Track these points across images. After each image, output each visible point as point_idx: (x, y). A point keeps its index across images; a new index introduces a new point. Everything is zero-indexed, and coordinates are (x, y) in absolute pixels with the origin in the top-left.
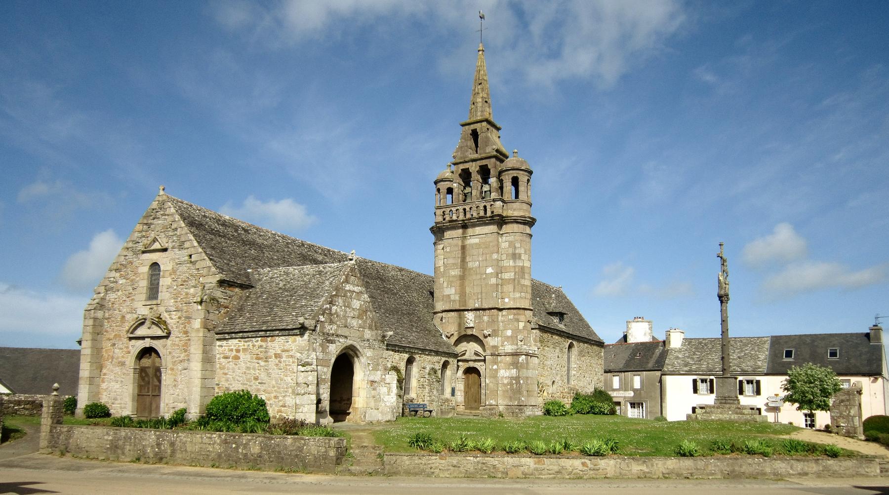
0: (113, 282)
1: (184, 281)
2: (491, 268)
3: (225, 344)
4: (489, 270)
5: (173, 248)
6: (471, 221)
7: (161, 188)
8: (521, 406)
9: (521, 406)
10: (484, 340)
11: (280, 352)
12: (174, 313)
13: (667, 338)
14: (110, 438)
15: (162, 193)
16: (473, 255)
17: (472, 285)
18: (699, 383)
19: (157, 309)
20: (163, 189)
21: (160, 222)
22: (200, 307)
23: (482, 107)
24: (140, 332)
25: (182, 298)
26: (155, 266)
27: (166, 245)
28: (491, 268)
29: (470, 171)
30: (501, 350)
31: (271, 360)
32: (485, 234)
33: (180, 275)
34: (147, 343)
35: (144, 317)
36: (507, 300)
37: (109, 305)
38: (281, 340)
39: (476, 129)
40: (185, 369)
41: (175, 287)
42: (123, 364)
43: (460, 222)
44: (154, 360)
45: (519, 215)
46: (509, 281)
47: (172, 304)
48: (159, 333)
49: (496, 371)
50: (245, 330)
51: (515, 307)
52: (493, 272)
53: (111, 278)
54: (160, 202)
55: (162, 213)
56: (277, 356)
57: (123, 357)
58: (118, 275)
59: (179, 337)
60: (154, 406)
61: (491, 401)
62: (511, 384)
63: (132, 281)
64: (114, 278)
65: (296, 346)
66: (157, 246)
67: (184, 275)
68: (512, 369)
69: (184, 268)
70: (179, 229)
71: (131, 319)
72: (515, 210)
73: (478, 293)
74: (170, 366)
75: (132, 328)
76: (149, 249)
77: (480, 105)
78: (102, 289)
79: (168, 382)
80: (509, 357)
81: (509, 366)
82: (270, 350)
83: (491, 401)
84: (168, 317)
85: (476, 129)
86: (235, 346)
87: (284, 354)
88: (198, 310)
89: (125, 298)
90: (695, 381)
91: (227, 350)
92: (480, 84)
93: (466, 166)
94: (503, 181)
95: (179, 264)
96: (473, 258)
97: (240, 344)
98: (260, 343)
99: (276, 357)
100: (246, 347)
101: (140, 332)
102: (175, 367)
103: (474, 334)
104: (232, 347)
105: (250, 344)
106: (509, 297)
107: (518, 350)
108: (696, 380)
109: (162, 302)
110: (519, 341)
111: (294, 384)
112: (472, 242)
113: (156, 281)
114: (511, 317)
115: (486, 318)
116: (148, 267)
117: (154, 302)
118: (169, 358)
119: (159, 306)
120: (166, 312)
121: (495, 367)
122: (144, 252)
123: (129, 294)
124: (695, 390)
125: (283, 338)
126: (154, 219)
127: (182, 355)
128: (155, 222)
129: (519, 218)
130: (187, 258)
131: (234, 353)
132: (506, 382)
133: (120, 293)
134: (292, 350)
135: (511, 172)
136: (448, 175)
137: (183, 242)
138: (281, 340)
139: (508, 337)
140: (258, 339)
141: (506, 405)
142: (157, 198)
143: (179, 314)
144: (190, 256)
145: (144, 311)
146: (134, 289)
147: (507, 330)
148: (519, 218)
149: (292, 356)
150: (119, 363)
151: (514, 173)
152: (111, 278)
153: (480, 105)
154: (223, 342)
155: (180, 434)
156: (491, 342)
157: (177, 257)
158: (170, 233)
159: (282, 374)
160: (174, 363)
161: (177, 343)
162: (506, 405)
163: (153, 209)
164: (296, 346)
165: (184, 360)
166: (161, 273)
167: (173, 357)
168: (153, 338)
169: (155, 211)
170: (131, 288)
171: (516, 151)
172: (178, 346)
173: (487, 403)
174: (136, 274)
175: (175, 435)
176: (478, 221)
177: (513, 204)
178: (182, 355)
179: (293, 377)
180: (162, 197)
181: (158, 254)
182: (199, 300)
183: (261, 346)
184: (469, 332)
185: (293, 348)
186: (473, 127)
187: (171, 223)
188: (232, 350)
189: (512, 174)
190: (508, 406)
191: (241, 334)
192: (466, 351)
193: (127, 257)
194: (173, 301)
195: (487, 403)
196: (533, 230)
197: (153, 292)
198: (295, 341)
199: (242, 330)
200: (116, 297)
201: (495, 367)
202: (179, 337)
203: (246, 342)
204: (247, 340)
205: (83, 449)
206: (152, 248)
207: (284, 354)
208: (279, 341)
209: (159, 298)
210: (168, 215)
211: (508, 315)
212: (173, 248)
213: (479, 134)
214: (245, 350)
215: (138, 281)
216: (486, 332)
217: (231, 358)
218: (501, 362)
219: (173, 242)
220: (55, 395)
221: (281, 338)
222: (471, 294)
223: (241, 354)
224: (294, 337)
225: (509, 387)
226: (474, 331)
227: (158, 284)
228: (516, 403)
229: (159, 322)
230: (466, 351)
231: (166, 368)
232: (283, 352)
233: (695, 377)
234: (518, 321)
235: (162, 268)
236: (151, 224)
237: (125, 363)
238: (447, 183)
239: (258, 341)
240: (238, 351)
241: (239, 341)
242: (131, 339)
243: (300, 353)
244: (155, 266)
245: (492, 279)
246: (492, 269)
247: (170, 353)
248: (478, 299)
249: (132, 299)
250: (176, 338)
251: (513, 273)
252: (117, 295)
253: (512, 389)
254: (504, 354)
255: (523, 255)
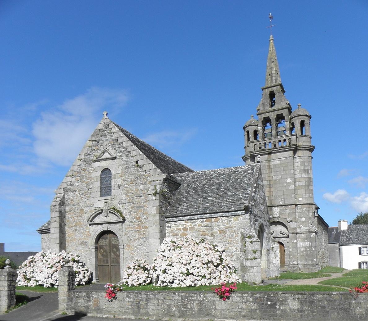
0: (71, 185)
1: (134, 180)
2: (290, 179)
3: (173, 225)
4: (289, 181)
5: (121, 156)
6: (275, 149)
7: (105, 113)
8: (313, 264)
9: (313, 264)
10: (288, 225)
11: (224, 229)
12: (127, 204)
13: (339, 225)
14: (131, 300)
15: (105, 117)
16: (276, 172)
17: (277, 190)
18: (362, 249)
19: (111, 203)
20: (107, 114)
21: (107, 138)
22: (154, 198)
23: (276, 76)
24: (96, 220)
25: (132, 193)
26: (106, 171)
27: (114, 155)
28: (290, 179)
29: (270, 118)
30: (298, 230)
31: (217, 235)
32: (285, 158)
33: (129, 176)
34: (105, 228)
35: (100, 209)
36: (300, 199)
37: (69, 202)
38: (224, 220)
39: (273, 91)
40: (140, 245)
41: (126, 186)
42: (85, 244)
43: (267, 151)
44: (110, 240)
45: (306, 145)
46: (301, 187)
47: (124, 198)
48: (115, 219)
49: (296, 243)
50: (191, 214)
51: (307, 203)
52: (291, 181)
53: (68, 182)
54: (105, 124)
55: (108, 131)
56: (221, 232)
57: (84, 239)
58: (74, 180)
59: (132, 222)
60: (113, 273)
61: (294, 262)
62: (306, 251)
63: (87, 183)
64: (71, 182)
65: (238, 223)
66: (106, 155)
67: (134, 176)
68: (306, 242)
69: (133, 170)
70: (124, 143)
71: (88, 213)
72: (303, 142)
73: (281, 195)
74: (126, 243)
75: (92, 217)
76: (99, 159)
77: (274, 75)
78: (62, 191)
79: (125, 255)
80: (304, 234)
81: (304, 240)
82: (215, 228)
83: (294, 262)
84: (121, 207)
85: (273, 91)
86: (182, 226)
87: (228, 231)
88: (153, 200)
89: (82, 196)
90: (360, 249)
91: (175, 229)
92: (273, 62)
93: (267, 115)
94: (294, 123)
95: (128, 168)
96: (276, 173)
97: (187, 225)
98: (205, 223)
99: (220, 233)
100: (193, 226)
101: (96, 220)
102: (131, 244)
103: (280, 221)
104: (180, 227)
105: (196, 224)
106: (302, 197)
107: (310, 230)
108: (360, 247)
109: (116, 197)
110: (310, 224)
111: (238, 252)
112: (275, 163)
113: (109, 182)
114: (304, 209)
115: (288, 211)
116: (101, 172)
117: (109, 197)
118: (125, 238)
119: (113, 200)
120: (119, 204)
121: (295, 241)
122: (96, 161)
123: (85, 193)
124: (360, 254)
125: (226, 218)
126: (101, 136)
127: (137, 235)
128: (103, 138)
129: (307, 147)
130: (134, 163)
131: (182, 232)
132: (302, 249)
133: (77, 193)
134: (235, 227)
135: (300, 117)
136: (253, 120)
137: (130, 152)
138: (224, 220)
139: (303, 222)
140: (203, 220)
141: (303, 264)
142: (102, 121)
143: (132, 205)
144: (137, 162)
145: (101, 205)
146: (88, 189)
147: (302, 218)
148: (307, 147)
149: (235, 232)
150: (81, 243)
151: (303, 118)
152: (68, 182)
153: (274, 75)
154: (172, 224)
155: (207, 295)
156: (292, 225)
157: (125, 163)
158: (117, 146)
159: (227, 245)
160: (130, 241)
161: (131, 226)
162: (303, 264)
163: (99, 130)
164: (238, 223)
165: (139, 238)
166: (113, 176)
167: (129, 236)
168: (109, 223)
169: (101, 131)
170: (87, 189)
171: (300, 104)
172: (133, 228)
173: (291, 263)
174: (89, 178)
175: (202, 296)
176: (280, 149)
177: (302, 138)
178: (137, 235)
179: (237, 247)
180: (107, 120)
181: (107, 161)
182: (154, 192)
183: (207, 226)
184: (276, 220)
185: (236, 225)
186: (270, 90)
187: (116, 138)
188: (180, 229)
189: (301, 118)
190: (304, 264)
191: (188, 217)
192: (273, 232)
193: (81, 166)
194: (124, 196)
195: (291, 263)
196: (313, 154)
197: (106, 190)
198: (237, 220)
199: (188, 214)
200: (74, 195)
201: (295, 241)
202: (132, 222)
203: (193, 223)
204: (193, 221)
205: (104, 310)
206: (103, 157)
207: (228, 231)
208: (222, 221)
209: (112, 194)
210: (114, 133)
211: (302, 208)
212: (121, 156)
213: (275, 94)
214: (191, 229)
215: (92, 183)
216: (289, 220)
217: (179, 235)
218: (299, 237)
219: (121, 152)
220: (8, 268)
221: (224, 218)
222: (276, 196)
223: (188, 232)
224: (237, 217)
225: (305, 253)
226: (280, 219)
227: (110, 184)
228: (310, 263)
229: (115, 211)
230: (273, 232)
231: (123, 245)
232: (227, 228)
233: (360, 246)
234: (309, 212)
235: (113, 172)
236: (99, 140)
237: (87, 242)
238: (253, 127)
239: (203, 221)
240: (185, 230)
241: (186, 222)
242: (90, 225)
243: (243, 229)
244: (106, 171)
245: (291, 186)
246: (291, 180)
247: (125, 234)
248: (281, 199)
249: (88, 196)
250: (130, 222)
251: (304, 182)
252: (75, 194)
253: (307, 254)
254: (301, 233)
255: (309, 170)
